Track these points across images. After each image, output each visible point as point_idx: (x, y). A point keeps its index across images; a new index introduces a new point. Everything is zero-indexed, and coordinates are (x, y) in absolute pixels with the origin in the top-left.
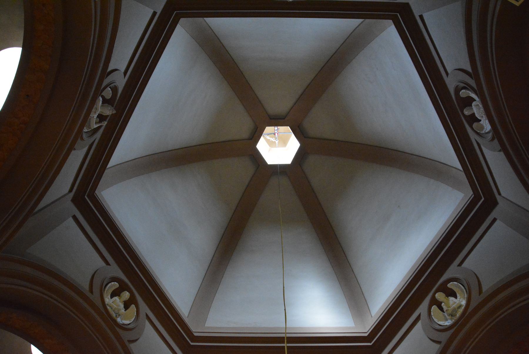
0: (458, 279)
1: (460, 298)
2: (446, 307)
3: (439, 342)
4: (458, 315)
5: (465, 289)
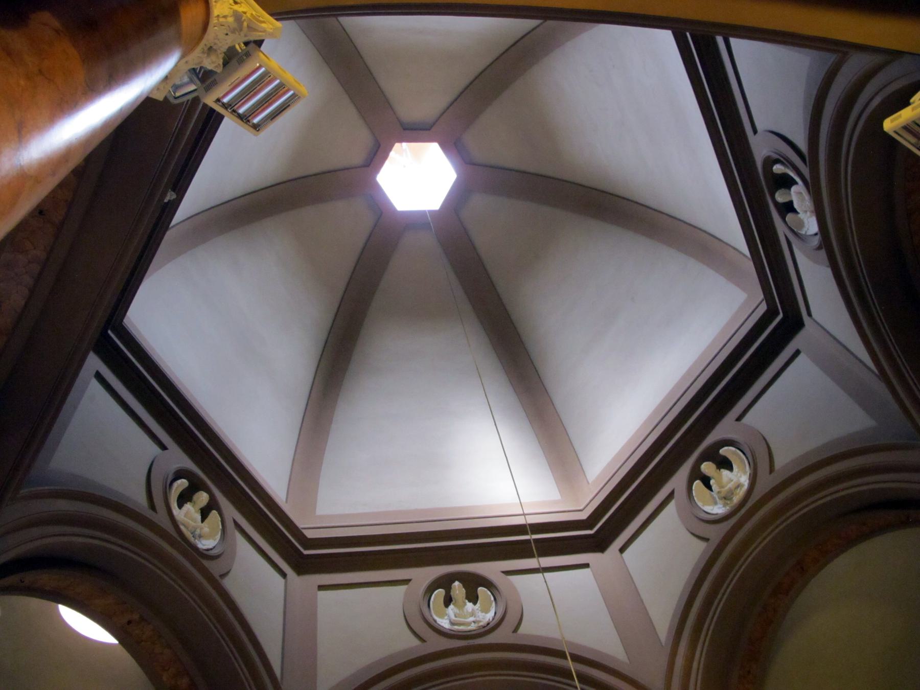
0: (734, 441)
1: (738, 472)
2: (718, 487)
3: (706, 540)
4: (736, 499)
5: (747, 458)
